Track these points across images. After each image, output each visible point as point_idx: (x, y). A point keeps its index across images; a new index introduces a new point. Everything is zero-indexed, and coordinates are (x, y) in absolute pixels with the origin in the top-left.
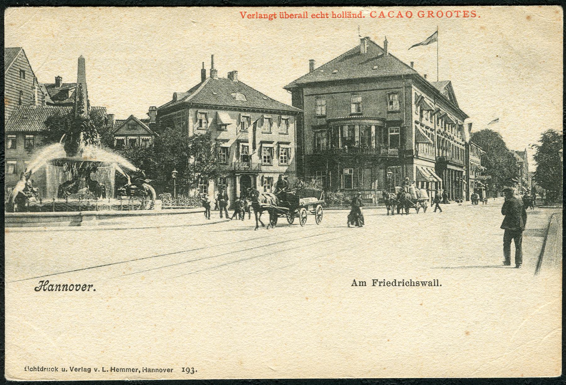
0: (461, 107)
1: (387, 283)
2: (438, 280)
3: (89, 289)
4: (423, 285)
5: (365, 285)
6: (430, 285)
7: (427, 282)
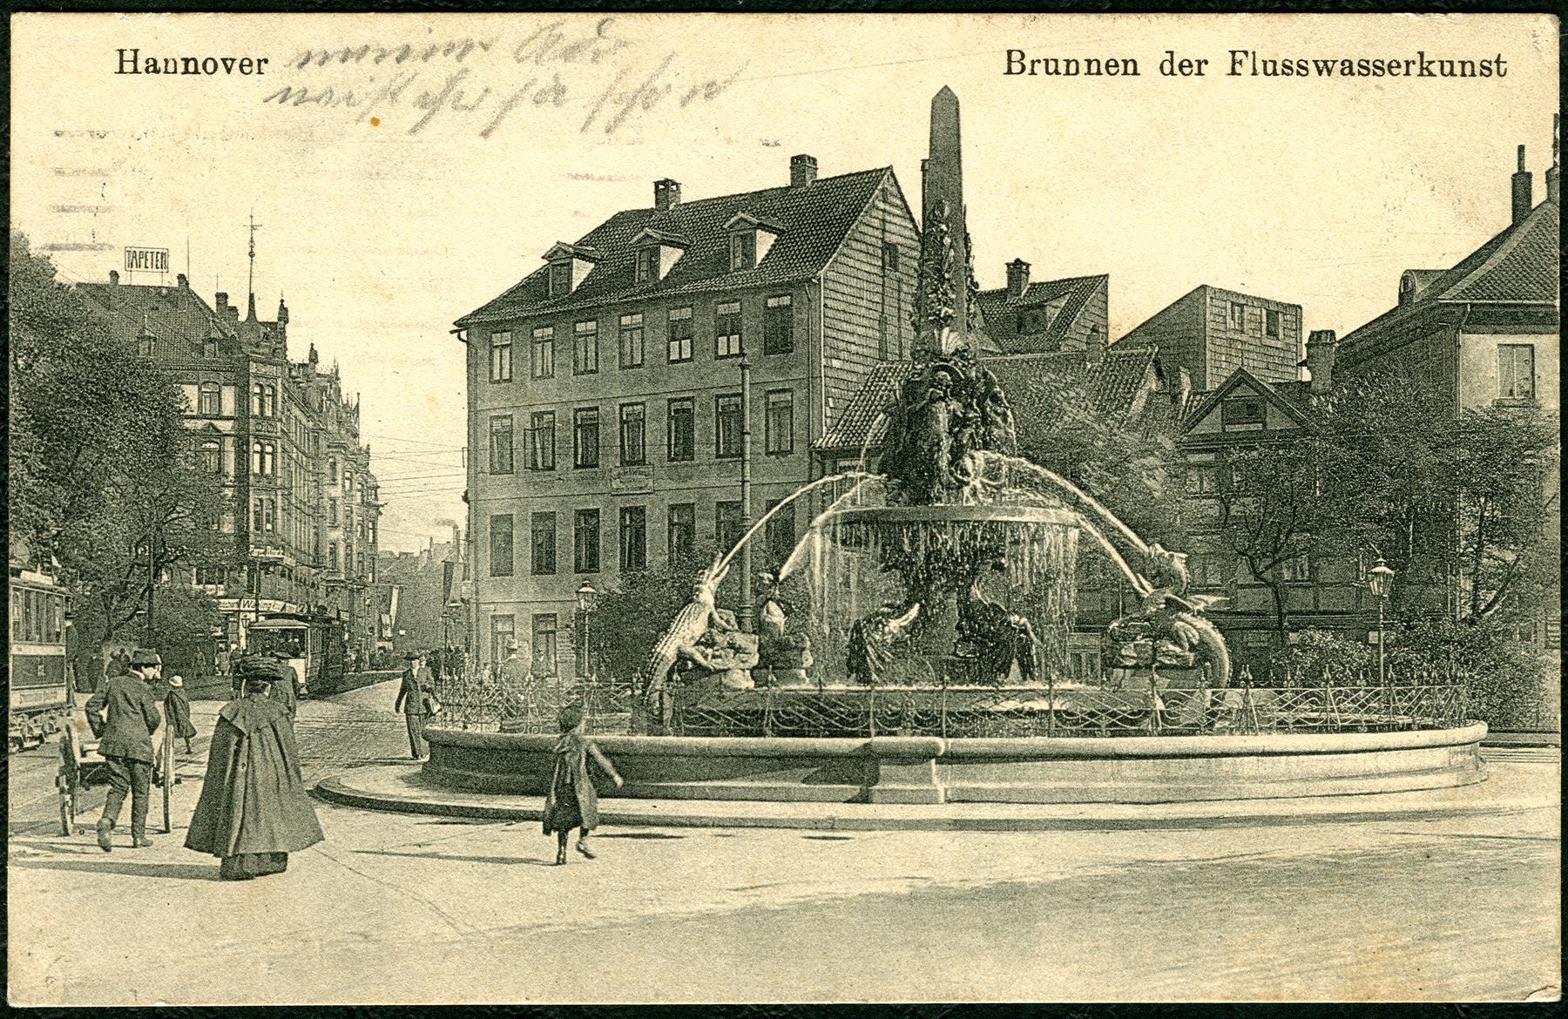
0: (1449, 263)
1: (1107, 66)
2: (1254, 53)
3: (1033, 70)
4: (1320, 73)
5: (1135, 73)
6: (1347, 71)
7: (1334, 62)
